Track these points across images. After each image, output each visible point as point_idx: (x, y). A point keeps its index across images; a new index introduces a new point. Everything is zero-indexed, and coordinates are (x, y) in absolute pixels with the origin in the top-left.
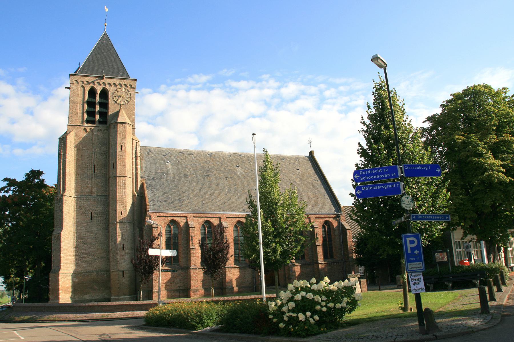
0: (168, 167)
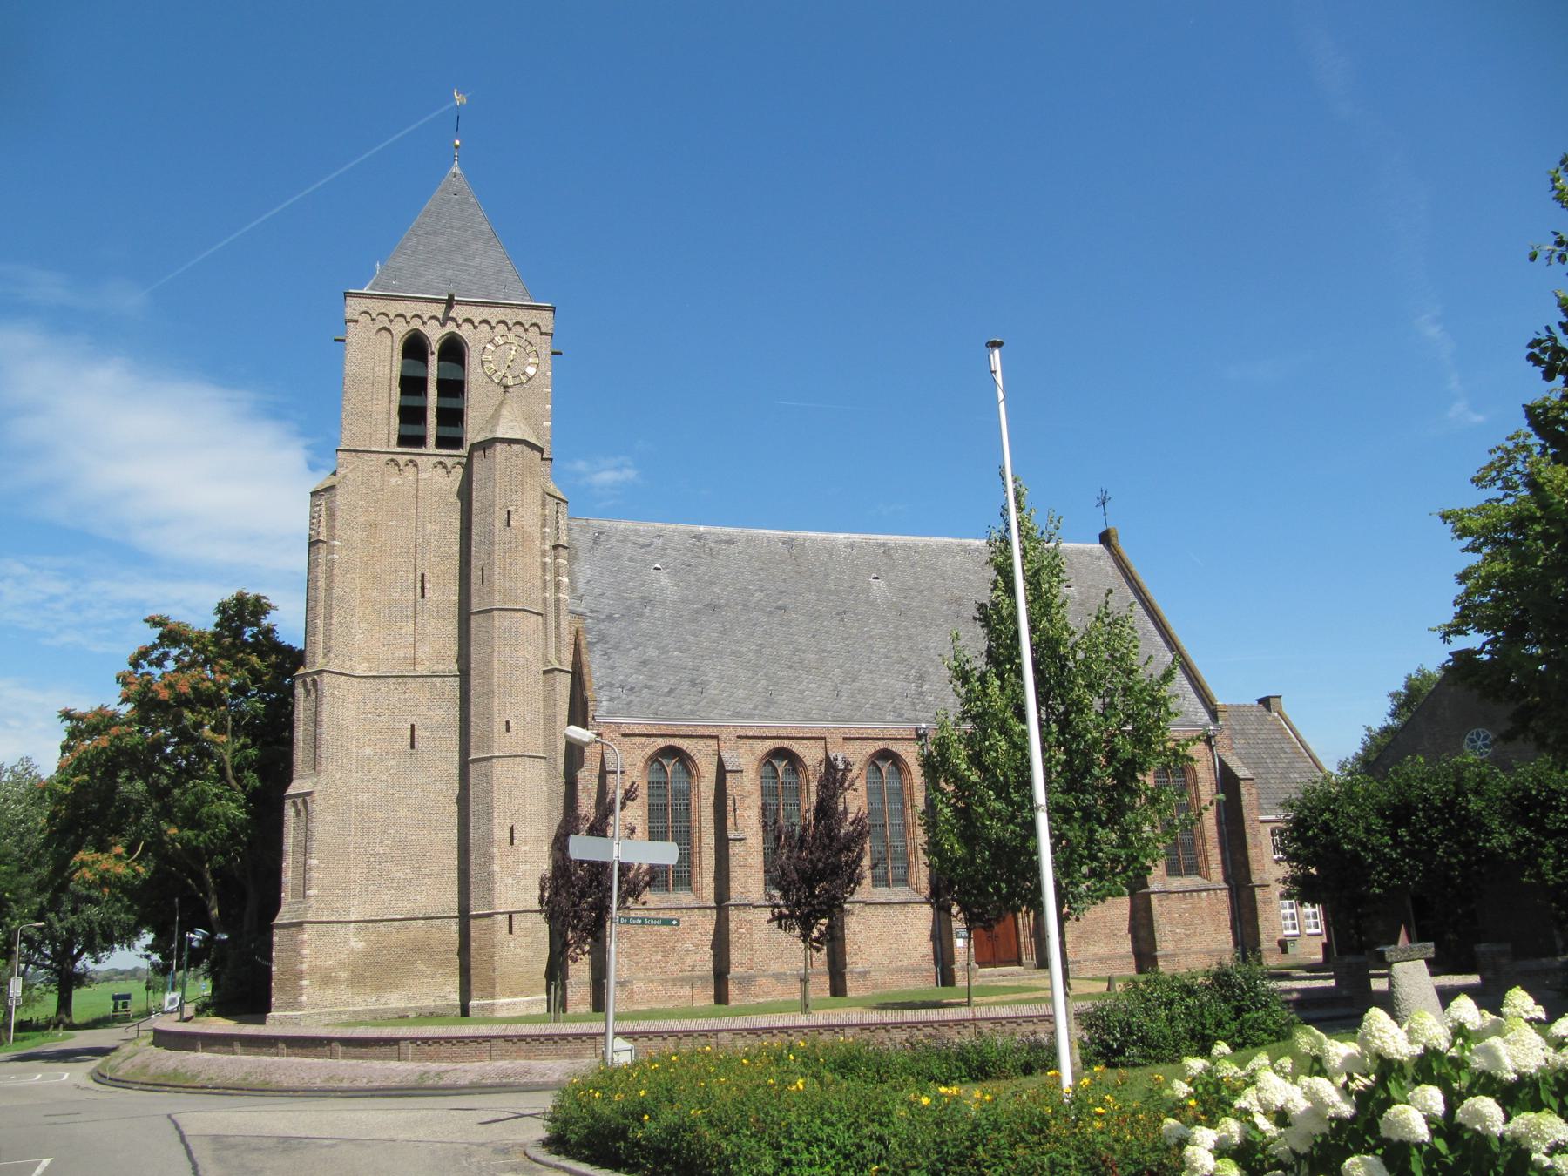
0: (658, 580)
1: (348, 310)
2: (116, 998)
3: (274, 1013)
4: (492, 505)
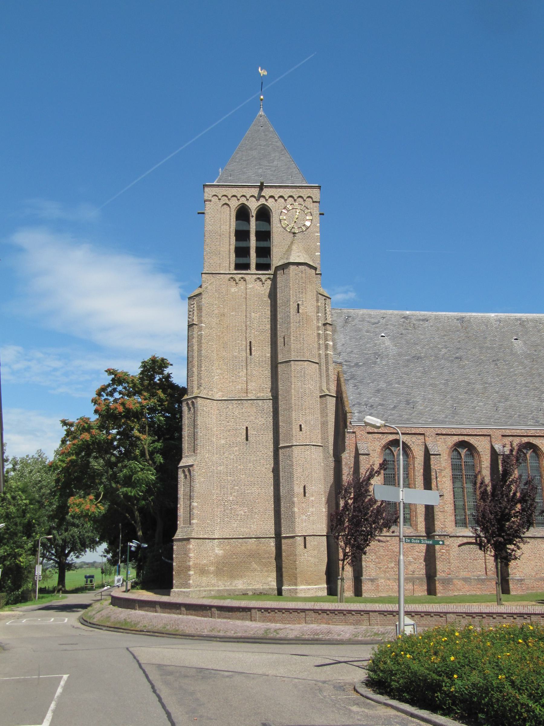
1: (206, 194)
2: (86, 577)
3: (174, 590)
4: (289, 301)
